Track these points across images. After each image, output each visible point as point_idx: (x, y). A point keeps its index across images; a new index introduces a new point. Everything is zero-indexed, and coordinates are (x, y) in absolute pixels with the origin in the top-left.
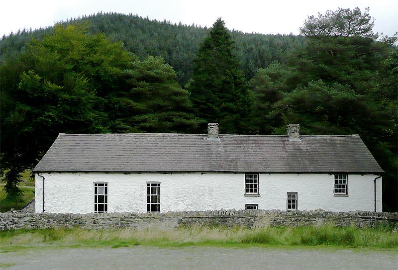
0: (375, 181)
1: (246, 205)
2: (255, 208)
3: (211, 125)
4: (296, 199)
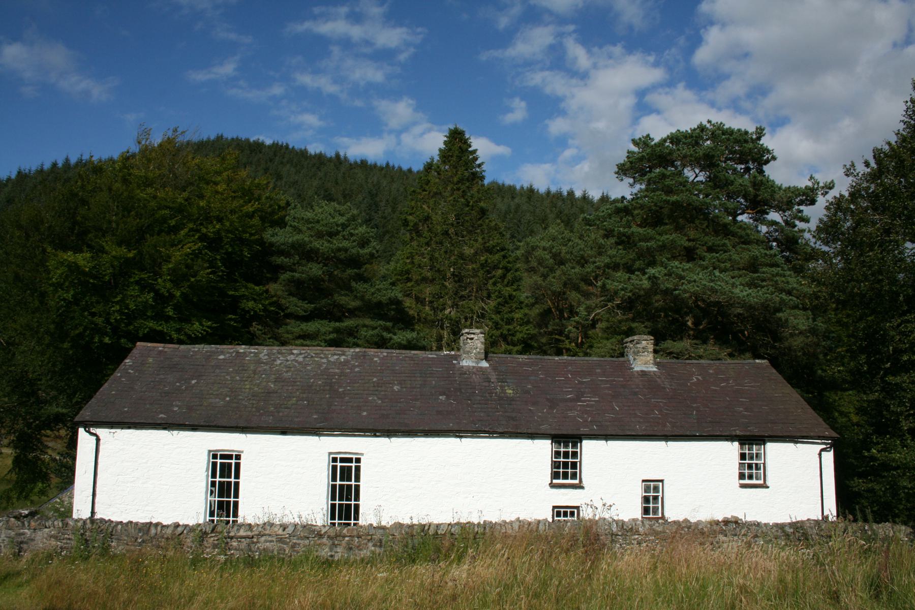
0: (820, 455)
1: (554, 507)
2: (572, 514)
3: (468, 333)
4: (660, 494)
